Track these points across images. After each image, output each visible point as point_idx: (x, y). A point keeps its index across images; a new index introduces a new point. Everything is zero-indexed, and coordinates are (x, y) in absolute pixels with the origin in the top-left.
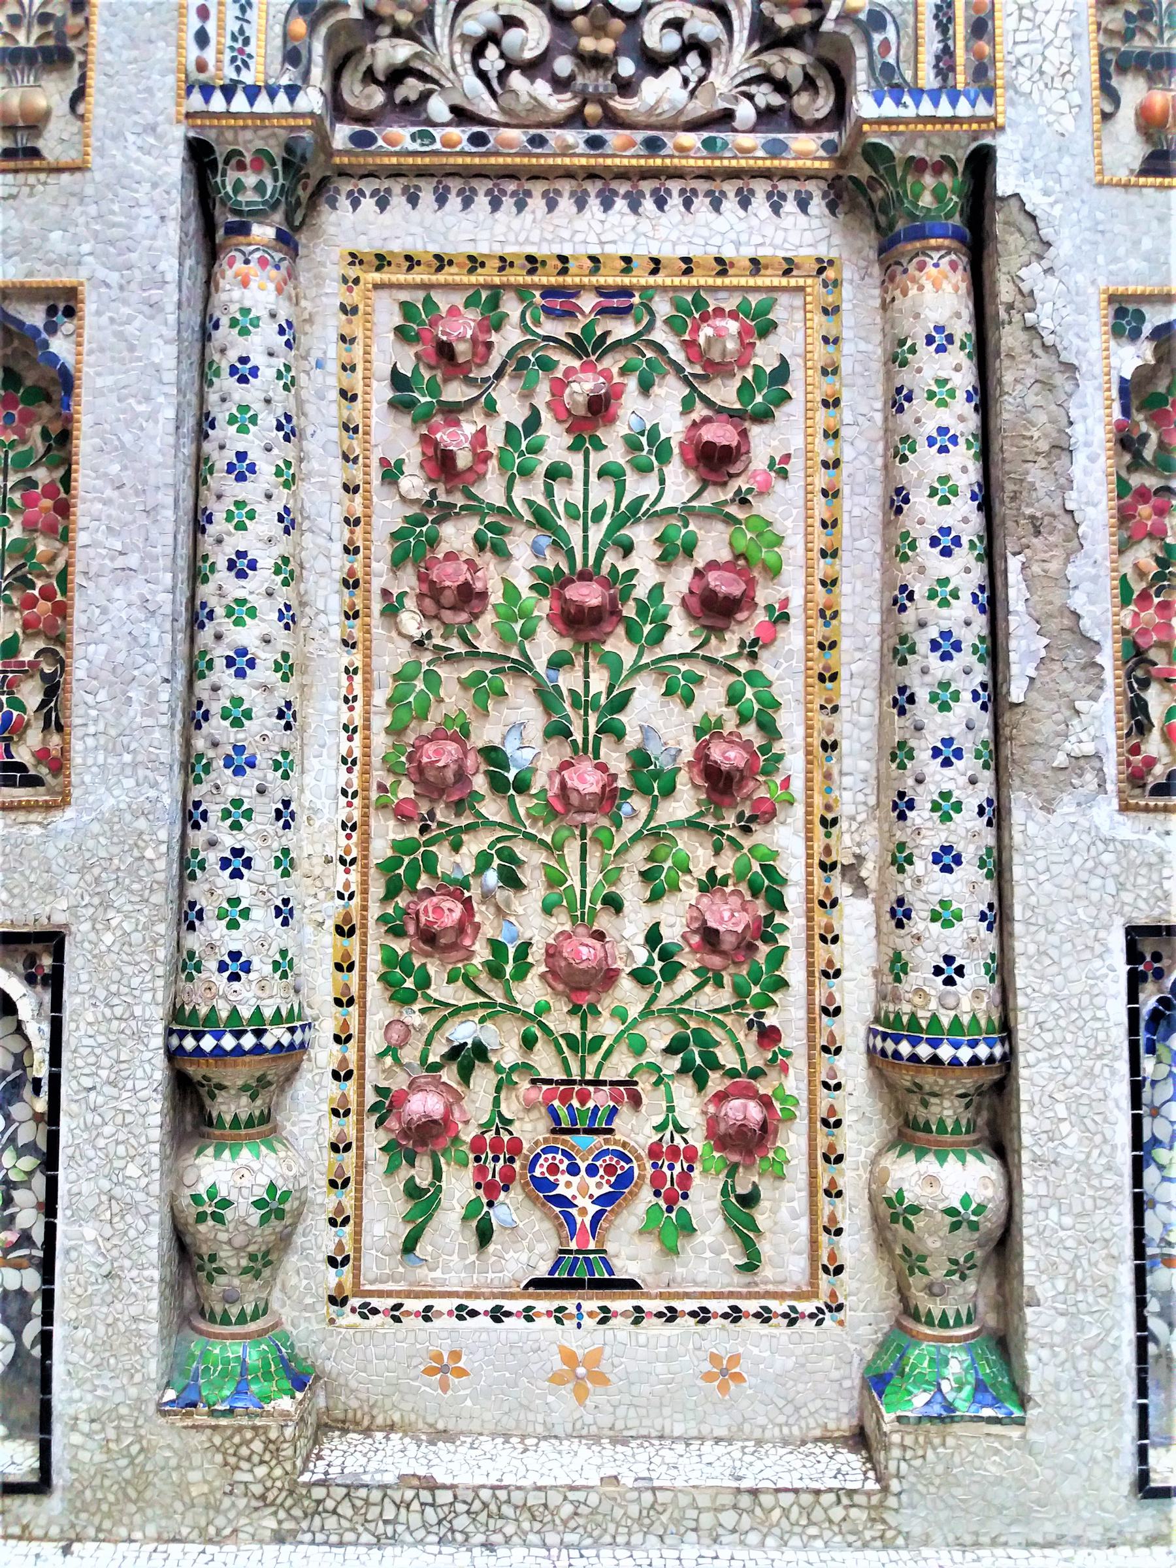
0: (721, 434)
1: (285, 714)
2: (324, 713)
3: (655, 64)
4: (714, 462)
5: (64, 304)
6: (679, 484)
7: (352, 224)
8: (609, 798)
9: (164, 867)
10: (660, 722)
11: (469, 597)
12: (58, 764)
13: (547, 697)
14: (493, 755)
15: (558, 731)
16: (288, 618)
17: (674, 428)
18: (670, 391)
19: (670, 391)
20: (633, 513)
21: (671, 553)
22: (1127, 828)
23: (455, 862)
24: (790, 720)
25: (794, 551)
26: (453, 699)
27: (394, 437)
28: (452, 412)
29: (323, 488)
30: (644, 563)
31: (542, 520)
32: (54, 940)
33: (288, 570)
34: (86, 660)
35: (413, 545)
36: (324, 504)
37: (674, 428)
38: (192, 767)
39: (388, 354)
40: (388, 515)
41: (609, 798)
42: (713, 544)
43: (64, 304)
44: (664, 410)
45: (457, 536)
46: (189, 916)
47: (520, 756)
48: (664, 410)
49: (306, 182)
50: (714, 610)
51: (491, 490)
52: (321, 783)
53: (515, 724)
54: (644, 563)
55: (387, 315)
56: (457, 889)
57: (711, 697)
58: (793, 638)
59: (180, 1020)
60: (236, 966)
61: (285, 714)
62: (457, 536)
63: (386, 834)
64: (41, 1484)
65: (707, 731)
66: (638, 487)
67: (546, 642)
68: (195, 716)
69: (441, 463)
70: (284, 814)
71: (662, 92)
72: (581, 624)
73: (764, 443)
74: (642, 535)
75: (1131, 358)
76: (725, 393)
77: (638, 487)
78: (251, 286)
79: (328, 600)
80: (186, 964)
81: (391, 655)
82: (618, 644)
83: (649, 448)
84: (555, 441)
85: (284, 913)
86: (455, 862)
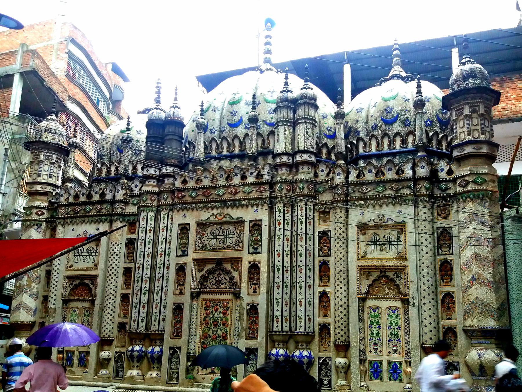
0: (225, 312)
1: (195, 332)
2: (198, 332)
3: (222, 284)
4: (224, 314)
5: (183, 304)
6: (222, 315)
7: (203, 296)
8: (216, 338)
9: (187, 343)
10: (220, 332)
11: (208, 323)
12: (181, 335)
13: (213, 330)
14: (209, 335)
15: (213, 333)
16: (196, 325)
17: (222, 311)
18: (222, 308)
19: (222, 308)
20: (219, 317)
21: (221, 320)
22: (246, 341)
23: (206, 343)
24: (228, 332)
25: (229, 320)
26: (207, 331)
27: (204, 312)
28: (208, 310)
29: (198, 317)
30: (219, 321)
31: (213, 317)
32: (180, 347)
33: (196, 322)
34: (183, 328)
35: (205, 320)
36: (199, 316)
37: (222, 311)
38: (189, 336)
39: (204, 306)
40: (203, 317)
41: (216, 338)
42: (224, 319)
43: (183, 304)
44: (221, 310)
45: (207, 319)
46: (188, 346)
47: (211, 335)
48: (221, 310)
49: (198, 294)
50: (224, 325)
51: (210, 316)
52: (198, 337)
53: (210, 333)
54: (219, 321)
55: (204, 303)
56: (206, 344)
57: (223, 331)
58: (229, 326)
59: (188, 353)
60: (191, 349)
61: (195, 332)
62: (207, 319)
63: (202, 340)
64: (178, 384)
65: (223, 333)
66: (219, 315)
67: (213, 326)
68: (190, 332)
69: (206, 314)
70: (195, 339)
71: (222, 286)
72: (215, 326)
73: (228, 312)
74: (219, 319)
75: (248, 308)
76: (225, 309)
77: (219, 315)
78: (195, 303)
79: (199, 323)
80: (188, 349)
81: (203, 327)
82: (218, 327)
83: (220, 313)
84: (214, 311)
85: (195, 346)
86: (206, 343)
